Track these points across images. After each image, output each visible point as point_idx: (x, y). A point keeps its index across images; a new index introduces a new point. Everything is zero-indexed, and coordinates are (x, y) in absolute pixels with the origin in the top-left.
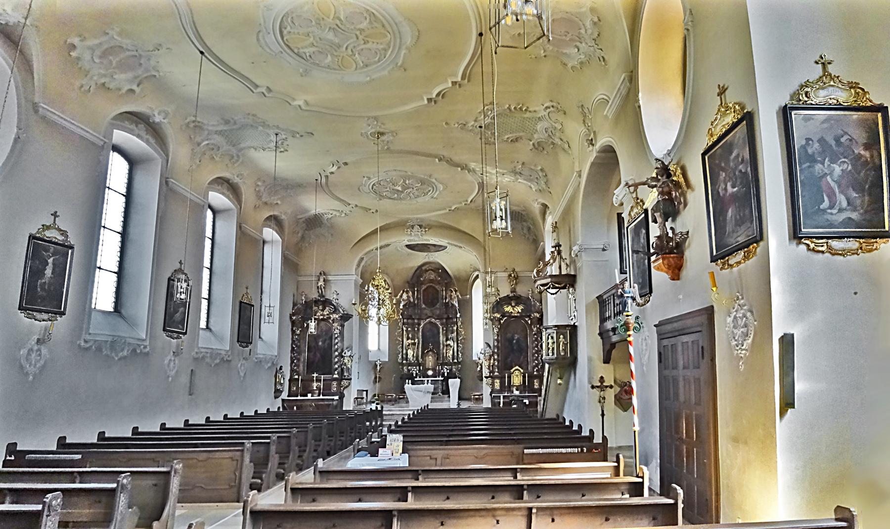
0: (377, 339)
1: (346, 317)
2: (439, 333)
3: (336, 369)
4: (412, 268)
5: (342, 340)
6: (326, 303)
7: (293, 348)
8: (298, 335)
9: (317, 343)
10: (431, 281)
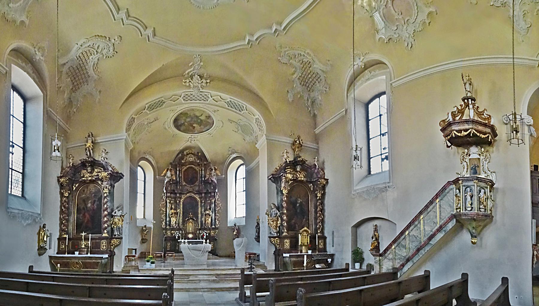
0: (144, 211)
1: (116, 177)
2: (198, 205)
3: (106, 228)
4: (174, 151)
5: (112, 200)
6: (94, 164)
7: (61, 209)
8: (67, 197)
9: (86, 205)
10: (192, 163)
